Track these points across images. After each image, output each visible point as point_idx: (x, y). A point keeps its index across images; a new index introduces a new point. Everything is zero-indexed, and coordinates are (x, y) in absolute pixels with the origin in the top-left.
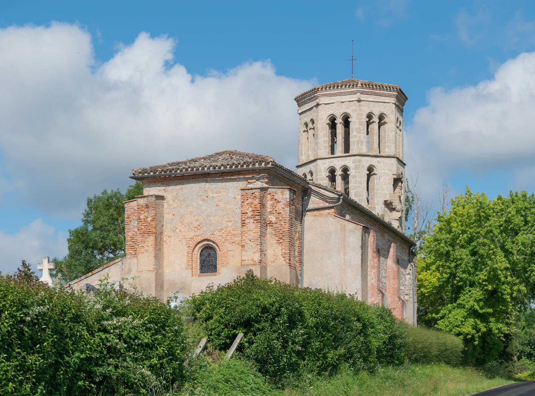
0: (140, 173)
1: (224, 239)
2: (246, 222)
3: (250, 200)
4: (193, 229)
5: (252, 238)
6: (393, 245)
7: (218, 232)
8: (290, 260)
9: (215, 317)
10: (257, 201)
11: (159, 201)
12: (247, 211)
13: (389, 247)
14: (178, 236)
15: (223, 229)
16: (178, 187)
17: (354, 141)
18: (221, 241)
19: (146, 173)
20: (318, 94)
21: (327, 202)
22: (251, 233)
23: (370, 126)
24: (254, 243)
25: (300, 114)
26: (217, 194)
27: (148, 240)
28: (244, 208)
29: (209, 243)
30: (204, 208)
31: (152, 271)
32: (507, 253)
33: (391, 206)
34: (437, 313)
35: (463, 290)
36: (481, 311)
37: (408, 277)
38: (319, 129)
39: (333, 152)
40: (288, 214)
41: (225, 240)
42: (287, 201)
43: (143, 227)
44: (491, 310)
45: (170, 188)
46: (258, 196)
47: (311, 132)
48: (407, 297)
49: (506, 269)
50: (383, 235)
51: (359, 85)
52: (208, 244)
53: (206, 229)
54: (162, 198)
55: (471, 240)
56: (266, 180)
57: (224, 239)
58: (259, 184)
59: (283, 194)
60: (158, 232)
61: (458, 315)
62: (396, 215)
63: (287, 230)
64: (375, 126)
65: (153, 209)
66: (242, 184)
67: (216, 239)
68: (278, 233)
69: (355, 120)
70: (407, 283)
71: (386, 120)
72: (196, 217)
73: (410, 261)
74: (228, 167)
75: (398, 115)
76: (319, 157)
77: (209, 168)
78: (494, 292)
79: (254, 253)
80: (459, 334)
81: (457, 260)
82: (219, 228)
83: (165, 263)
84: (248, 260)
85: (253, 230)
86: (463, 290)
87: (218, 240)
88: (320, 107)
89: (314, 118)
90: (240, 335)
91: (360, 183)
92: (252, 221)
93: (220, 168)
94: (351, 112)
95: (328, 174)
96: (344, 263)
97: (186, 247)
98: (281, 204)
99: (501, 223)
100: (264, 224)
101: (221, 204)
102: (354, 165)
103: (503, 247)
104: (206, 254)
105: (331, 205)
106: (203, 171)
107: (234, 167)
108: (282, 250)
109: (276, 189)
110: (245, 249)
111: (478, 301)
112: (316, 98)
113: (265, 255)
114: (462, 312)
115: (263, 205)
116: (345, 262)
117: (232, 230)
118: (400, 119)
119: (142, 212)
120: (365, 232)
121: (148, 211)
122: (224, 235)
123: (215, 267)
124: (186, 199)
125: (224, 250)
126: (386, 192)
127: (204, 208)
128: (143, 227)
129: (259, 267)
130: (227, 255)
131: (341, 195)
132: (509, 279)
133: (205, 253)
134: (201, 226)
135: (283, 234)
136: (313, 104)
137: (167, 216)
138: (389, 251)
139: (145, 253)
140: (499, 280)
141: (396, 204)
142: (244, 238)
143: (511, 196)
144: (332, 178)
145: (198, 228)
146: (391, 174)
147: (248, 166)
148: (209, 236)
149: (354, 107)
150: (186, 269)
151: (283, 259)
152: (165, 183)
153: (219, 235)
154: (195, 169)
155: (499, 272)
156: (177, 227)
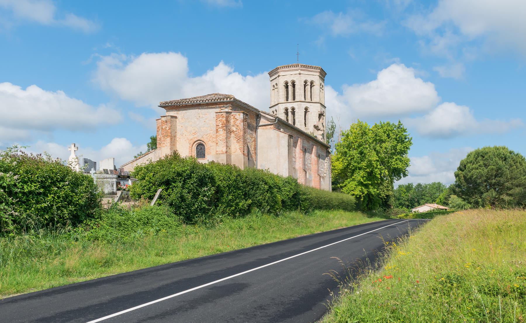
3: (220, 118)
6: (314, 147)
8: (244, 151)
9: (146, 178)
10: (224, 119)
11: (173, 119)
12: (219, 125)
13: (313, 148)
16: (184, 112)
21: (269, 121)
22: (220, 136)
23: (306, 87)
25: (271, 81)
29: (201, 142)
32: (378, 153)
33: (317, 128)
34: (343, 183)
35: (355, 171)
36: (364, 183)
37: (326, 164)
38: (280, 88)
39: (287, 99)
44: (370, 182)
45: (180, 112)
46: (225, 116)
47: (276, 90)
48: (325, 175)
49: (378, 161)
50: (308, 142)
51: (300, 66)
54: (176, 117)
55: (359, 146)
56: (231, 108)
58: (227, 110)
61: (353, 184)
62: (321, 132)
64: (308, 87)
66: (218, 110)
70: (325, 167)
71: (314, 84)
73: (327, 156)
74: (210, 100)
75: (321, 82)
77: (200, 101)
78: (372, 172)
79: (223, 147)
80: (353, 195)
81: (351, 156)
86: (355, 171)
88: (280, 77)
89: (277, 83)
91: (301, 116)
92: (222, 129)
93: (206, 101)
95: (284, 111)
97: (188, 144)
100: (229, 132)
103: (375, 150)
104: (200, 148)
105: (272, 123)
106: (197, 103)
107: (213, 101)
108: (239, 146)
111: (363, 177)
112: (278, 72)
113: (230, 148)
114: (356, 183)
115: (228, 121)
118: (323, 84)
120: (290, 138)
123: (204, 155)
126: (315, 120)
131: (277, 118)
132: (379, 167)
136: (276, 76)
137: (179, 127)
138: (312, 150)
140: (374, 166)
141: (320, 127)
142: (218, 139)
143: (381, 123)
144: (287, 113)
146: (317, 111)
147: (221, 100)
151: (240, 151)
152: (178, 109)
154: (192, 102)
155: (373, 162)
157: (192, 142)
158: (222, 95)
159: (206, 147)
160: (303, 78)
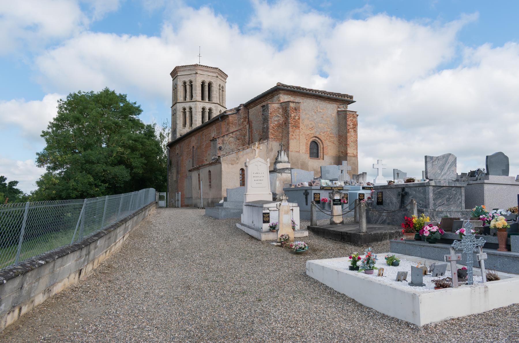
12: (350, 124)
17: (215, 96)
30: (315, 117)
72: (311, 122)
76: (197, 100)
82: (323, 131)
88: (197, 75)
101: (324, 117)
102: (215, 108)
121: (296, 112)
127: (315, 117)
128: (293, 122)
134: (314, 128)
149: (215, 80)
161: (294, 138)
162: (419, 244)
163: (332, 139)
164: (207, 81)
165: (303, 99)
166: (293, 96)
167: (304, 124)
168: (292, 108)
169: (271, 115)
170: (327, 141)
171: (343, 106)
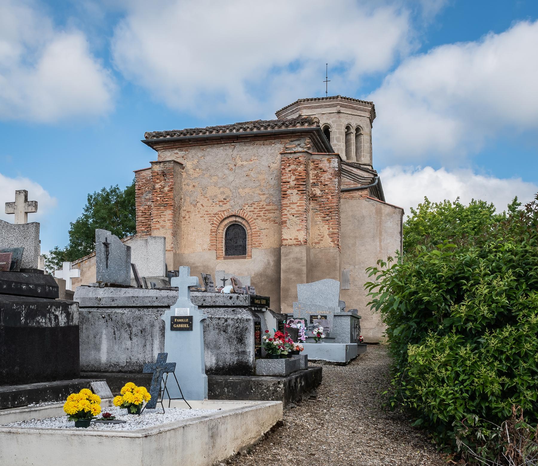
0: (154, 136)
1: (256, 215)
2: (287, 192)
3: (293, 167)
4: (218, 203)
5: (295, 212)
7: (249, 206)
10: (301, 168)
12: (289, 180)
14: (199, 212)
15: (254, 204)
18: (252, 218)
19: (161, 136)
20: (300, 106)
21: (359, 183)
22: (294, 206)
24: (298, 218)
26: (247, 163)
27: (164, 214)
28: (285, 176)
30: (231, 178)
31: (170, 251)
40: (337, 186)
41: (257, 216)
42: (336, 171)
43: (158, 198)
52: (236, 221)
53: (233, 203)
57: (256, 215)
59: (330, 162)
60: (176, 205)
63: (334, 204)
64: (353, 137)
65: (171, 177)
67: (246, 215)
68: (323, 208)
69: (336, 130)
71: (362, 132)
72: (222, 190)
79: (298, 230)
82: (250, 202)
83: (184, 242)
84: (291, 239)
85: (296, 203)
87: (248, 217)
90: (420, 351)
92: (295, 191)
94: (331, 123)
96: (380, 251)
98: (327, 173)
99: (476, 225)
101: (252, 174)
108: (329, 229)
109: (321, 156)
110: (286, 226)
116: (381, 249)
117: (266, 205)
119: (158, 181)
121: (165, 180)
122: (256, 210)
124: (210, 168)
125: (256, 228)
127: (231, 178)
128: (158, 198)
129: (305, 248)
130: (260, 234)
133: (232, 233)
134: (228, 200)
135: (330, 210)
139: (161, 229)
145: (224, 202)
148: (238, 211)
149: (334, 119)
150: (209, 250)
153: (250, 210)
156: (198, 200)
157: (216, 221)
158: (266, 122)
159: (248, 232)
160: (345, 122)
161: (162, 226)
162: (14, 411)
163: (271, 215)
164: (354, 124)
165: (203, 150)
166: (184, 149)
167: (208, 195)
168: (156, 174)
169: (140, 192)
170: (259, 221)
171: (297, 143)
